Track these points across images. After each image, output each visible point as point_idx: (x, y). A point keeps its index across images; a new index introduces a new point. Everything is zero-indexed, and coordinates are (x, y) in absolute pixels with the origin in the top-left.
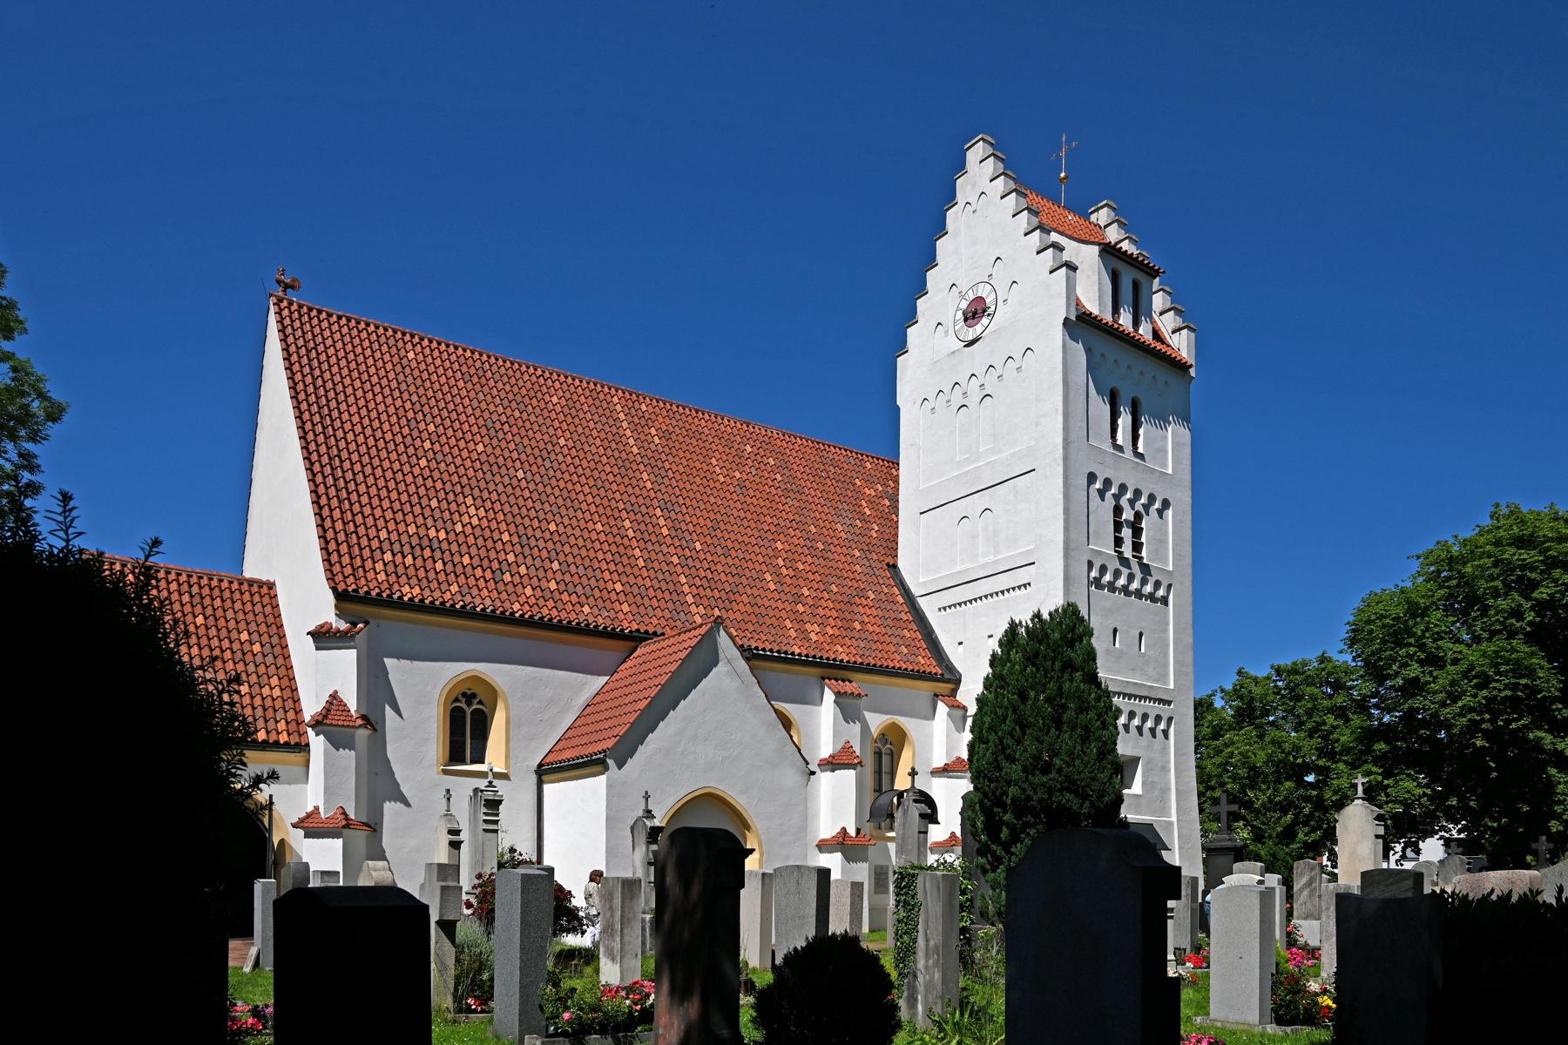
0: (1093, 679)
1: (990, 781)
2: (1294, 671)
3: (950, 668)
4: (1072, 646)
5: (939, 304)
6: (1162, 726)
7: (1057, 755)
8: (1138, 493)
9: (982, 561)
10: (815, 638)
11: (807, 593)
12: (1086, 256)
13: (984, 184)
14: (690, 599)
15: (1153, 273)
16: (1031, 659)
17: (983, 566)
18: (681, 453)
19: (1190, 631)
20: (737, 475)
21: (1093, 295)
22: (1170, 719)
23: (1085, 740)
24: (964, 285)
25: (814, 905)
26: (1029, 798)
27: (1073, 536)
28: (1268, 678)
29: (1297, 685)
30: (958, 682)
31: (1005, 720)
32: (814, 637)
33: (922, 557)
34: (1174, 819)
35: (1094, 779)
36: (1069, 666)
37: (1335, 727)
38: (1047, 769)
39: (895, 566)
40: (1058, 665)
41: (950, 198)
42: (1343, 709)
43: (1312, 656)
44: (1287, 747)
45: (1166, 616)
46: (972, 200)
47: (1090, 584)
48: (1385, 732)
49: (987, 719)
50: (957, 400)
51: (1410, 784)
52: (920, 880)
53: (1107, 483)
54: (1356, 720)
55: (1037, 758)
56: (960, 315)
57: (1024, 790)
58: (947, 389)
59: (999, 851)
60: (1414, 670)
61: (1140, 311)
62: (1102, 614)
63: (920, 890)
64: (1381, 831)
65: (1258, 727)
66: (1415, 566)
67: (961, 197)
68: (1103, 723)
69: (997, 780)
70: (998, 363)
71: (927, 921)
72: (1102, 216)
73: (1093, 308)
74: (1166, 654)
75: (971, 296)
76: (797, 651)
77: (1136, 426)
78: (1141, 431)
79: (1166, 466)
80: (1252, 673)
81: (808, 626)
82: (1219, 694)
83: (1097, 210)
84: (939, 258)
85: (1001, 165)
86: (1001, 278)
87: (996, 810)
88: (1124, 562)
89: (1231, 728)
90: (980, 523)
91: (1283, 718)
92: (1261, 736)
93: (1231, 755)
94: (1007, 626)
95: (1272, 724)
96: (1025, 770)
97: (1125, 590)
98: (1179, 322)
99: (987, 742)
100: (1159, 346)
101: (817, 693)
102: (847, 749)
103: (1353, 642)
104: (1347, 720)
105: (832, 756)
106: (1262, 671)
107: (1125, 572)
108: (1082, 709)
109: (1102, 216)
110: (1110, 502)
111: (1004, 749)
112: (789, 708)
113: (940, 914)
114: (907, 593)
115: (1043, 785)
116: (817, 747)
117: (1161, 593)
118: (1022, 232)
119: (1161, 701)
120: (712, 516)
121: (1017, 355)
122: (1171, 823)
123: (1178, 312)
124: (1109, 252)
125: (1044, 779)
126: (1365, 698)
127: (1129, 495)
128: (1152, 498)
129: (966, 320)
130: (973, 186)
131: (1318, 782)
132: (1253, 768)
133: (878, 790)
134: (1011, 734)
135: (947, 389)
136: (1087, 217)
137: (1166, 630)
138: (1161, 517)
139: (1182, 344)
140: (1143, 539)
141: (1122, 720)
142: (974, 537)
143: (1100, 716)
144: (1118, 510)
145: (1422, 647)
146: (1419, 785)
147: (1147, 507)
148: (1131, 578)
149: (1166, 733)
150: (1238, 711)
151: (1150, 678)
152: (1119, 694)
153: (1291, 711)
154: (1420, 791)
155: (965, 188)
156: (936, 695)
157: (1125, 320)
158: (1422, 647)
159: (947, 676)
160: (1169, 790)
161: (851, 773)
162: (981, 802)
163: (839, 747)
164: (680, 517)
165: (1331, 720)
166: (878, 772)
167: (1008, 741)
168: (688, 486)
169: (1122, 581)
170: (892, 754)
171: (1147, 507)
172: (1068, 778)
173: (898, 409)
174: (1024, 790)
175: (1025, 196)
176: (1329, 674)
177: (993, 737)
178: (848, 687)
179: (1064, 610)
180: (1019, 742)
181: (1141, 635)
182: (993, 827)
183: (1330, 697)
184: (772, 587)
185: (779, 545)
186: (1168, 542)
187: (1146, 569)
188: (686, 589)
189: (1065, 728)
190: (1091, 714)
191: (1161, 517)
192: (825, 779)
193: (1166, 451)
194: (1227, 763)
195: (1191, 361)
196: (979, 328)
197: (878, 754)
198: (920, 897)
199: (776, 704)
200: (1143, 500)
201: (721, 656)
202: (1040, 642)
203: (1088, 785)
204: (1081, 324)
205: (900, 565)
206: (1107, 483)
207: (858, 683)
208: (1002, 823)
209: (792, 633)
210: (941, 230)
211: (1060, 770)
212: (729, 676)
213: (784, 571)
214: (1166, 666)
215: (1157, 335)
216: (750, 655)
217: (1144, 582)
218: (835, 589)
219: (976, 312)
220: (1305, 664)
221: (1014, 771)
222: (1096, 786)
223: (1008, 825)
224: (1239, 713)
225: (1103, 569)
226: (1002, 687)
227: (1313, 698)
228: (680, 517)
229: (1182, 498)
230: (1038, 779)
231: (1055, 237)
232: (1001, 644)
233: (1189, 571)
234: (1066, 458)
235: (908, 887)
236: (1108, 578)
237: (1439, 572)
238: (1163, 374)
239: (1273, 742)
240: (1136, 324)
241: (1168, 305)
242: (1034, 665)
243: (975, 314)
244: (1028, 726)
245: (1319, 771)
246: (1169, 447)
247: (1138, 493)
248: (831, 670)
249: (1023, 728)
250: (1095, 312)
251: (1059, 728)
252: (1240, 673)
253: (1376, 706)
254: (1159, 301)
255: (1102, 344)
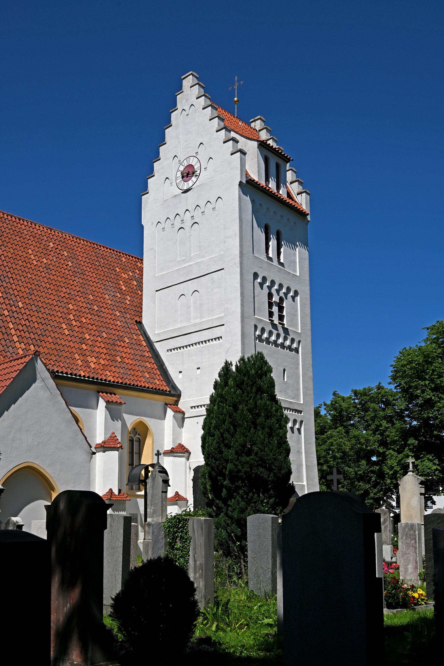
0: (273, 398)
1: (216, 459)
2: (365, 393)
3: (174, 387)
4: (261, 378)
5: (167, 167)
6: (297, 426)
7: (254, 444)
8: (281, 286)
9: (193, 322)
10: (92, 366)
11: (88, 337)
12: (251, 147)
13: (193, 100)
14: (15, 338)
15: (287, 160)
16: (239, 385)
17: (194, 325)
18: (10, 246)
19: (311, 369)
20: (45, 261)
21: (256, 172)
22: (301, 422)
23: (270, 435)
24: (182, 157)
25: (122, 540)
26: (239, 471)
27: (246, 310)
28: (350, 398)
29: (366, 402)
30: (179, 396)
31: (224, 423)
32: (93, 366)
33: (158, 317)
34: (305, 483)
35: (276, 459)
36: (260, 390)
37: (387, 428)
38: (249, 453)
39: (140, 323)
40: (254, 389)
41: (173, 106)
42: (391, 417)
43: (374, 385)
44: (363, 441)
45: (298, 360)
46: (187, 108)
47: (256, 339)
48: (413, 432)
49: (214, 422)
50: (178, 225)
51: (430, 464)
52: (190, 523)
53: (264, 279)
54: (398, 424)
55: (244, 446)
56: (179, 174)
57: (236, 466)
58: (172, 217)
59: (221, 504)
60: (429, 394)
61: (280, 181)
62: (274, 358)
63: (190, 529)
64: (423, 491)
65: (345, 427)
66: (425, 334)
67: (179, 106)
68: (280, 425)
69: (220, 460)
70: (202, 204)
71: (195, 549)
72: (258, 125)
73: (255, 178)
74: (298, 382)
75: (186, 164)
76: (83, 374)
77: (279, 247)
78: (282, 250)
79: (295, 271)
80: (342, 394)
81: (89, 358)
82: (323, 407)
83: (255, 121)
84: (167, 139)
85: (202, 90)
86: (203, 155)
87: (219, 478)
88: (274, 326)
89: (330, 428)
90: (192, 299)
91: (359, 422)
92: (347, 432)
93: (332, 444)
94: (223, 365)
95: (353, 425)
96: (237, 453)
97: (275, 343)
98: (301, 189)
99: (213, 436)
100: (288, 200)
101: (94, 402)
102: (113, 438)
103: (394, 378)
104: (393, 424)
105: (104, 442)
106: (347, 394)
107: (275, 332)
108: (268, 417)
109: (258, 125)
110: (266, 291)
111: (224, 440)
112: (76, 410)
113: (203, 544)
114: (148, 339)
115: (247, 463)
116: (94, 437)
117: (295, 346)
118: (215, 129)
119: (296, 411)
120: (29, 286)
121: (213, 200)
122: (303, 486)
123: (300, 183)
124: (263, 145)
125: (248, 459)
126: (402, 411)
127: (276, 287)
128: (289, 289)
129: (183, 177)
130: (187, 100)
131: (378, 461)
132: (344, 453)
133: (131, 464)
134: (228, 430)
135: (172, 217)
136: (249, 125)
137: (298, 368)
138: (294, 300)
139: (303, 201)
140: (284, 313)
141: (290, 425)
142: (189, 307)
143: (278, 420)
144: (270, 295)
145: (432, 381)
146: (434, 464)
147: (286, 294)
148: (278, 336)
149: (299, 430)
150: (334, 416)
151: (289, 397)
152: (288, 409)
153: (362, 418)
154: (435, 467)
155: (182, 101)
156: (166, 404)
157: (272, 185)
158: (432, 381)
159: (173, 392)
160: (301, 465)
161: (116, 453)
162: (210, 473)
163: (108, 436)
164: (9, 286)
165: (384, 423)
166: (131, 453)
167: (227, 435)
168: (14, 267)
169: (273, 338)
170: (139, 441)
171: (286, 294)
172: (261, 459)
173: (142, 227)
174: (236, 466)
175: (216, 109)
176: (383, 396)
177: (217, 433)
178: (113, 398)
179: (256, 357)
180: (233, 436)
181: (284, 370)
182: (216, 489)
183: (384, 410)
184: (67, 332)
185: (71, 306)
186: (298, 315)
187: (286, 331)
188: (13, 332)
189: (259, 428)
190: (274, 420)
191: (294, 300)
192: (99, 456)
193: (295, 262)
194: (330, 449)
195: (308, 212)
196: (190, 183)
197: (131, 441)
198: (190, 534)
199: (72, 408)
200: (284, 290)
201: (38, 376)
202: (244, 375)
203: (273, 463)
204: (248, 186)
205: (144, 322)
206: (264, 279)
207: (120, 396)
208: (222, 486)
209: (79, 362)
210: (168, 124)
211: (256, 454)
212: (43, 389)
213: (74, 323)
214: (298, 389)
215: (289, 195)
216: (55, 376)
217: (285, 339)
218: (104, 335)
219: (188, 173)
220: (370, 390)
221: (230, 454)
222: (277, 463)
223: (226, 487)
224: (335, 419)
225: (263, 330)
226: (222, 402)
227: (375, 411)
228: (9, 286)
229: (305, 289)
230: (244, 459)
231: (233, 134)
232: (220, 376)
233: (309, 333)
234: (241, 263)
235: (183, 527)
236: (265, 335)
237: (438, 338)
238: (293, 217)
239: (355, 437)
240: (278, 188)
241: (295, 179)
242: (241, 389)
243: (188, 174)
244: (240, 426)
245: (379, 455)
246: (297, 259)
247: (281, 286)
248: (103, 387)
249: (235, 427)
250: (256, 179)
251: (255, 428)
252: (334, 394)
253: (408, 416)
254: (290, 176)
255: (266, 202)
